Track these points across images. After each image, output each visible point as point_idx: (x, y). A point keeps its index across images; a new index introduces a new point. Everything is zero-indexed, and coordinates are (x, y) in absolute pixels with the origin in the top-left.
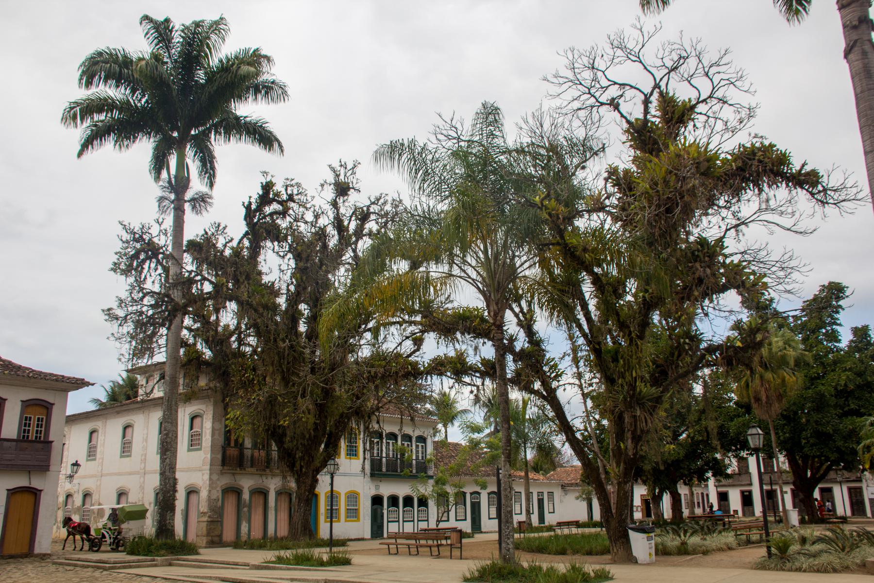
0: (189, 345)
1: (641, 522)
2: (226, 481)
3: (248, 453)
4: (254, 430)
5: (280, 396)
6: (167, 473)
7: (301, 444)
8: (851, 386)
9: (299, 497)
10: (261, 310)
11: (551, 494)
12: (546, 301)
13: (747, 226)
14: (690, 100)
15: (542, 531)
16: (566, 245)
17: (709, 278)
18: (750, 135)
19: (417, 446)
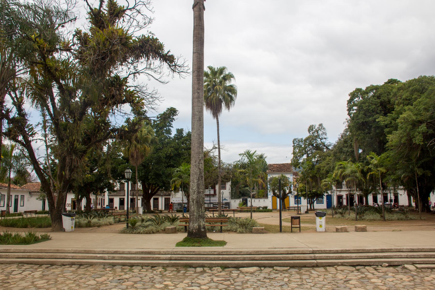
1: (70, 211)
8: (172, 154)
11: (23, 197)
12: (31, 93)
13: (139, 74)
14: (124, 6)
15: (15, 216)
16: (46, 65)
17: (117, 96)
18: (148, 31)
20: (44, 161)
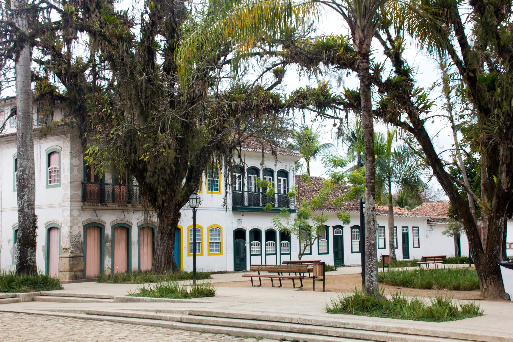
0: (41, 79)
2: (87, 216)
3: (109, 189)
4: (114, 166)
5: (140, 131)
6: (26, 210)
7: (163, 178)
9: (161, 231)
10: (115, 41)
15: (406, 266)
19: (279, 181)
20: (452, 158)
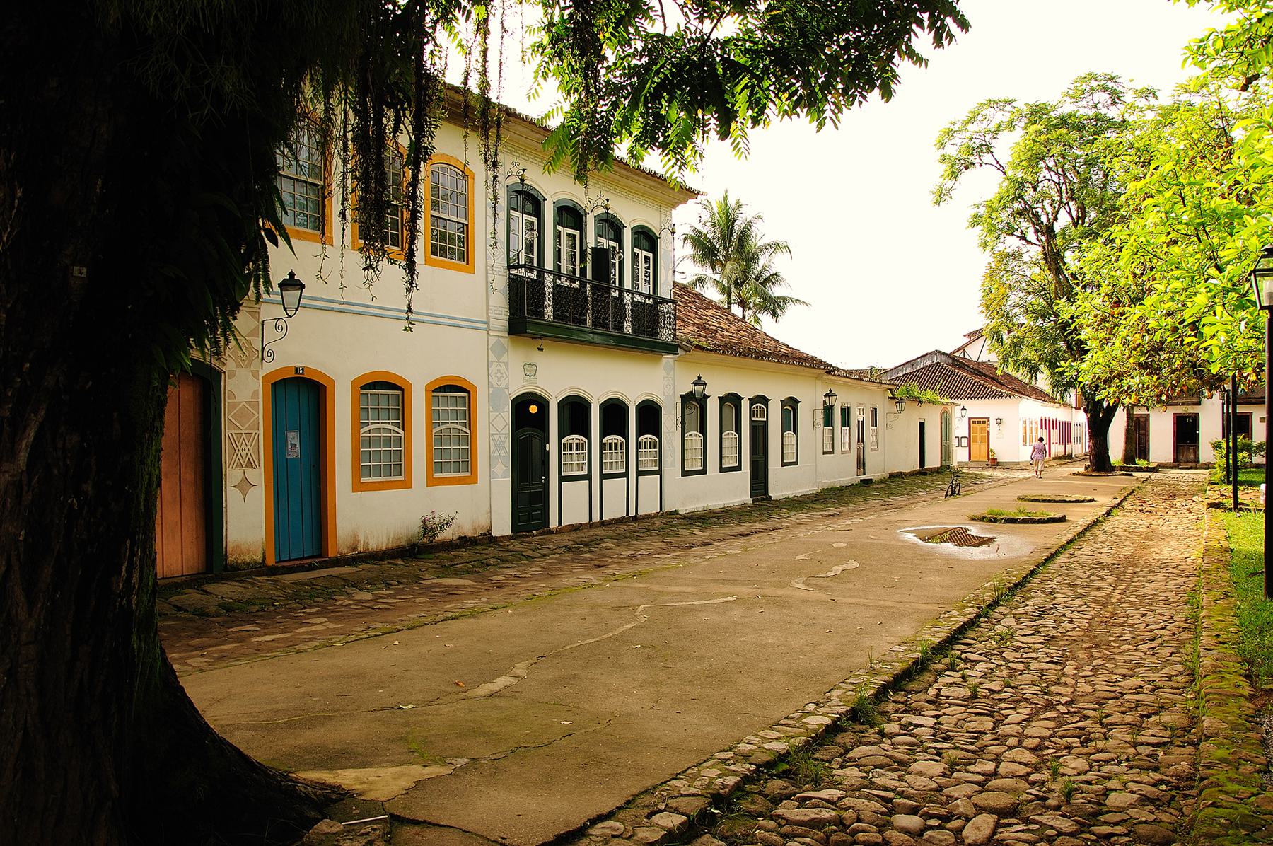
19: (635, 257)
